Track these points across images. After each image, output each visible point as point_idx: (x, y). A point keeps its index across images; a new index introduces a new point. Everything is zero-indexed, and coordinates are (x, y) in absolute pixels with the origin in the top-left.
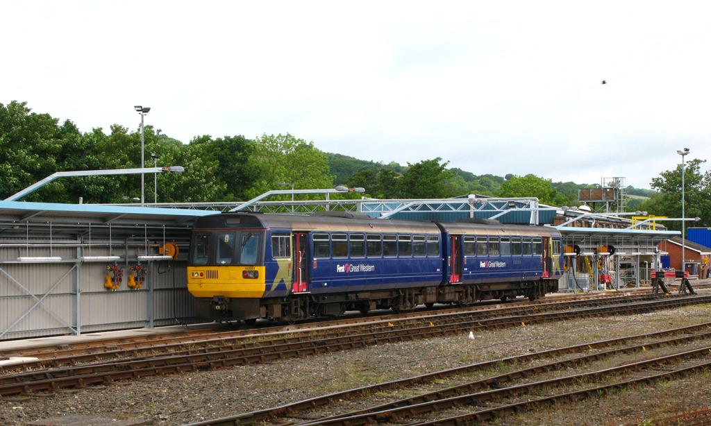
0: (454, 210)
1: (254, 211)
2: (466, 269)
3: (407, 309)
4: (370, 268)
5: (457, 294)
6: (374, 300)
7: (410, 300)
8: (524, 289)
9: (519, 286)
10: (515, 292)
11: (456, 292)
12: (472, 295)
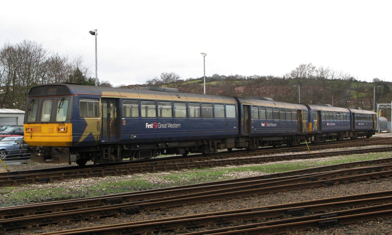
0: (388, 107)
1: (73, 83)
2: (253, 127)
3: (211, 153)
4: (275, 125)
5: (247, 143)
6: (182, 148)
7: (213, 147)
8: (287, 141)
9: (366, 132)
10: (282, 142)
11: (247, 141)
12: (256, 143)
